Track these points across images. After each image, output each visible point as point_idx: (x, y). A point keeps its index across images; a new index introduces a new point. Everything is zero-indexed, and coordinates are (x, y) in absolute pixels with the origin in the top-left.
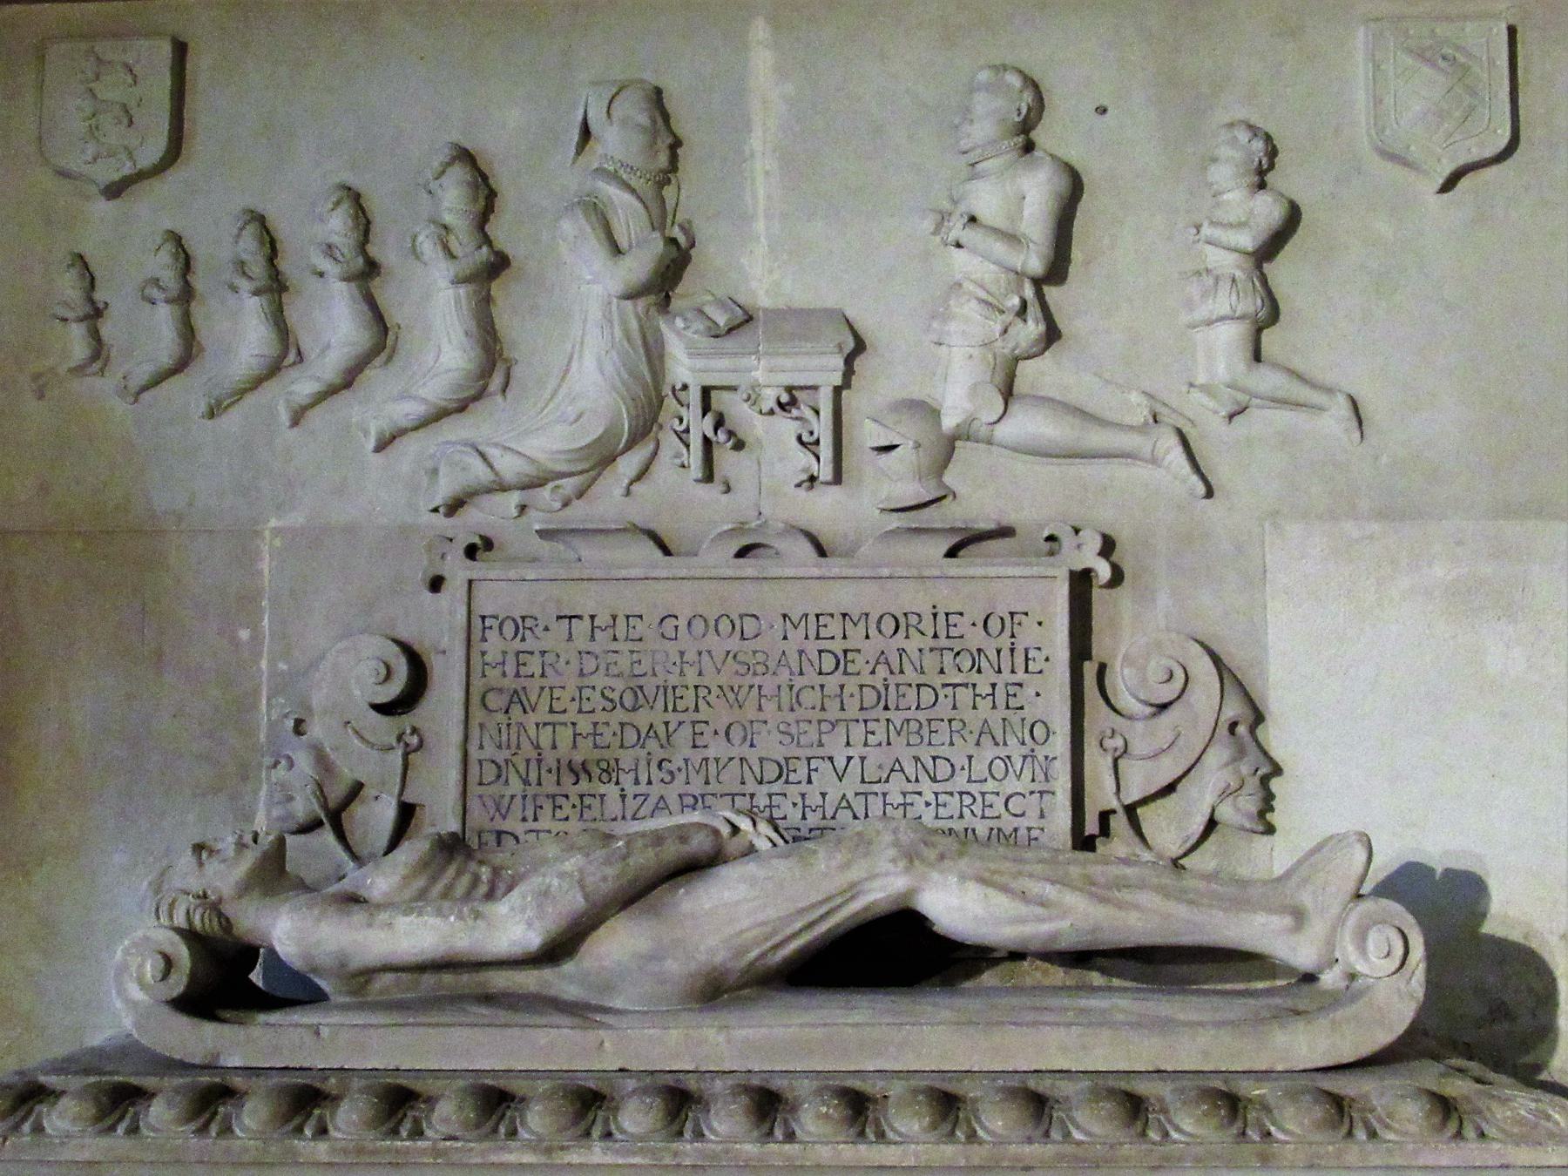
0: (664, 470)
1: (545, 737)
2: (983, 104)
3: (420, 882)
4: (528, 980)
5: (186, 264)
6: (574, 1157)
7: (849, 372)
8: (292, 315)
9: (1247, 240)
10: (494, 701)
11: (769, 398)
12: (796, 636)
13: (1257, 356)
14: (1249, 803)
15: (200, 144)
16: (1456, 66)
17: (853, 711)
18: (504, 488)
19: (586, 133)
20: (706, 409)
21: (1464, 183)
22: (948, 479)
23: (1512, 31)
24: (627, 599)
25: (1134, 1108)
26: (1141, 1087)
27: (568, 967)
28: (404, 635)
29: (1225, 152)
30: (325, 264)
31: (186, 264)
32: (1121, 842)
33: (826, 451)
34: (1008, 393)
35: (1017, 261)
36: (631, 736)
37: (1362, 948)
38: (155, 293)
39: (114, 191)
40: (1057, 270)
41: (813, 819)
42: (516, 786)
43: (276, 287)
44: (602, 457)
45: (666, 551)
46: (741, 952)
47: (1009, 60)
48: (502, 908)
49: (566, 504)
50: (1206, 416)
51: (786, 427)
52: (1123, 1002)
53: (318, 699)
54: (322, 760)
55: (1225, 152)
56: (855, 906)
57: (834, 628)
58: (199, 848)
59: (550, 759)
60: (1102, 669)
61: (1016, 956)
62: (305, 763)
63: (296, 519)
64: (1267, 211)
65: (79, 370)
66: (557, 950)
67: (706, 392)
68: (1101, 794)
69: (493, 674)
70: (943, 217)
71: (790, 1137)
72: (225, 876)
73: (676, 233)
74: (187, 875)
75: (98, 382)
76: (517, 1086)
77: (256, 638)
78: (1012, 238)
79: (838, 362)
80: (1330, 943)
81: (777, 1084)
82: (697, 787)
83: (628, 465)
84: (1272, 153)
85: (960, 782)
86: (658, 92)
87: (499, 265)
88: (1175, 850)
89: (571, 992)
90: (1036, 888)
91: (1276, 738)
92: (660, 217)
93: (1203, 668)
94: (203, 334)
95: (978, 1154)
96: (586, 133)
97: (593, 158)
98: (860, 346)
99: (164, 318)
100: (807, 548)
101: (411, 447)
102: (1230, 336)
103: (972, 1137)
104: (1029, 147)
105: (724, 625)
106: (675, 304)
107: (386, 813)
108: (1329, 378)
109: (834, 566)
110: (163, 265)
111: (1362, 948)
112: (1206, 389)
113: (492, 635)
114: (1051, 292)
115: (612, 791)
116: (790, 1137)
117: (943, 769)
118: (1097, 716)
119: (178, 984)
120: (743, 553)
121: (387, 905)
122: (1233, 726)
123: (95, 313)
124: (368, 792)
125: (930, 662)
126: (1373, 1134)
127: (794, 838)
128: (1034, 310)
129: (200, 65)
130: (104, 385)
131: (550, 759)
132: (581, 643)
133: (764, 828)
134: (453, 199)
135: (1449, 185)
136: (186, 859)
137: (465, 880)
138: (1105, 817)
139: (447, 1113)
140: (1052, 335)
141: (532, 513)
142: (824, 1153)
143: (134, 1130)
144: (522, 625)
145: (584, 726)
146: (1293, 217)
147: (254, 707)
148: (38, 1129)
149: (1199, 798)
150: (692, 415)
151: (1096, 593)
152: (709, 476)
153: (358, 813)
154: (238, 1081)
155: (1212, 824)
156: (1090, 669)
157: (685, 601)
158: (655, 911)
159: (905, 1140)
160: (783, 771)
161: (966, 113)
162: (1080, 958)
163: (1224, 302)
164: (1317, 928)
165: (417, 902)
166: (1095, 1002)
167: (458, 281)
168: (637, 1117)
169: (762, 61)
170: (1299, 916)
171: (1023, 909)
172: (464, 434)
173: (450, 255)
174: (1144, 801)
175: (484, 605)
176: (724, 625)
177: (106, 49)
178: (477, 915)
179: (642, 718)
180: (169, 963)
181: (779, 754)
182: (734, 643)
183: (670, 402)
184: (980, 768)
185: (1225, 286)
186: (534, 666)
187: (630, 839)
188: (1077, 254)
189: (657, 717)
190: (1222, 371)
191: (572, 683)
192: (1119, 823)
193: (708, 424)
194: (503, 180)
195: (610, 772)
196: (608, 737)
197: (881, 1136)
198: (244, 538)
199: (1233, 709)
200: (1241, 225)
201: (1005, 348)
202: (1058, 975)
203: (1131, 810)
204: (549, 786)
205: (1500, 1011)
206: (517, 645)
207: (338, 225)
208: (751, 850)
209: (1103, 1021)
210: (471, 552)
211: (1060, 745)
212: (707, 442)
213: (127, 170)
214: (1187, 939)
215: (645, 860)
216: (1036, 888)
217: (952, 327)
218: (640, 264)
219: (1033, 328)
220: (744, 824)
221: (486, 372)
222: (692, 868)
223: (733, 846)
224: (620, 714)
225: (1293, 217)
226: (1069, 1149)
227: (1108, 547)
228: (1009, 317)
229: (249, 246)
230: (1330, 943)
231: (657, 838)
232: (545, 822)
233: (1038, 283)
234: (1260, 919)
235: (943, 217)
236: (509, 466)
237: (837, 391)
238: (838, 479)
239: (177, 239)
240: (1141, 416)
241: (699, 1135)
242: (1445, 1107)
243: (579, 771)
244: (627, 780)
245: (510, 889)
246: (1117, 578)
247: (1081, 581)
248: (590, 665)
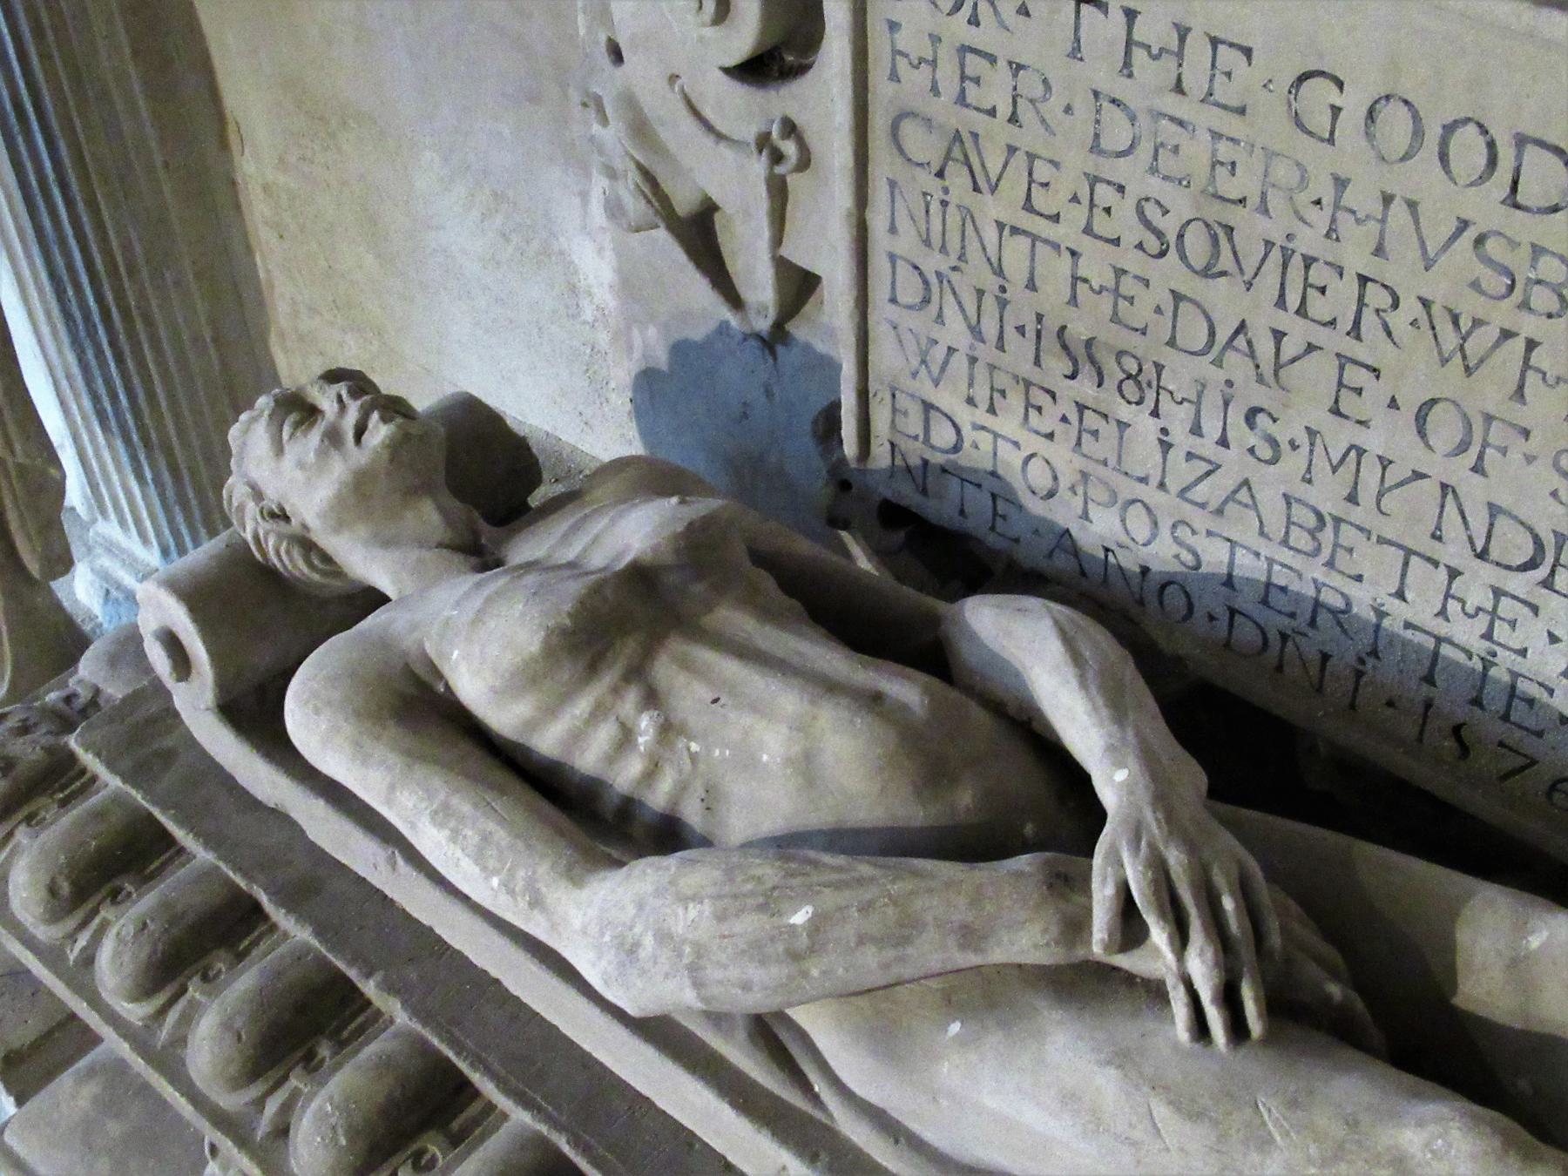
59: (1023, 308)
131: (1023, 308)
145: (1096, 268)
176: (1468, 150)
179: (1226, 301)
182: (1485, 206)
224: (1169, 273)
244: (1178, 418)
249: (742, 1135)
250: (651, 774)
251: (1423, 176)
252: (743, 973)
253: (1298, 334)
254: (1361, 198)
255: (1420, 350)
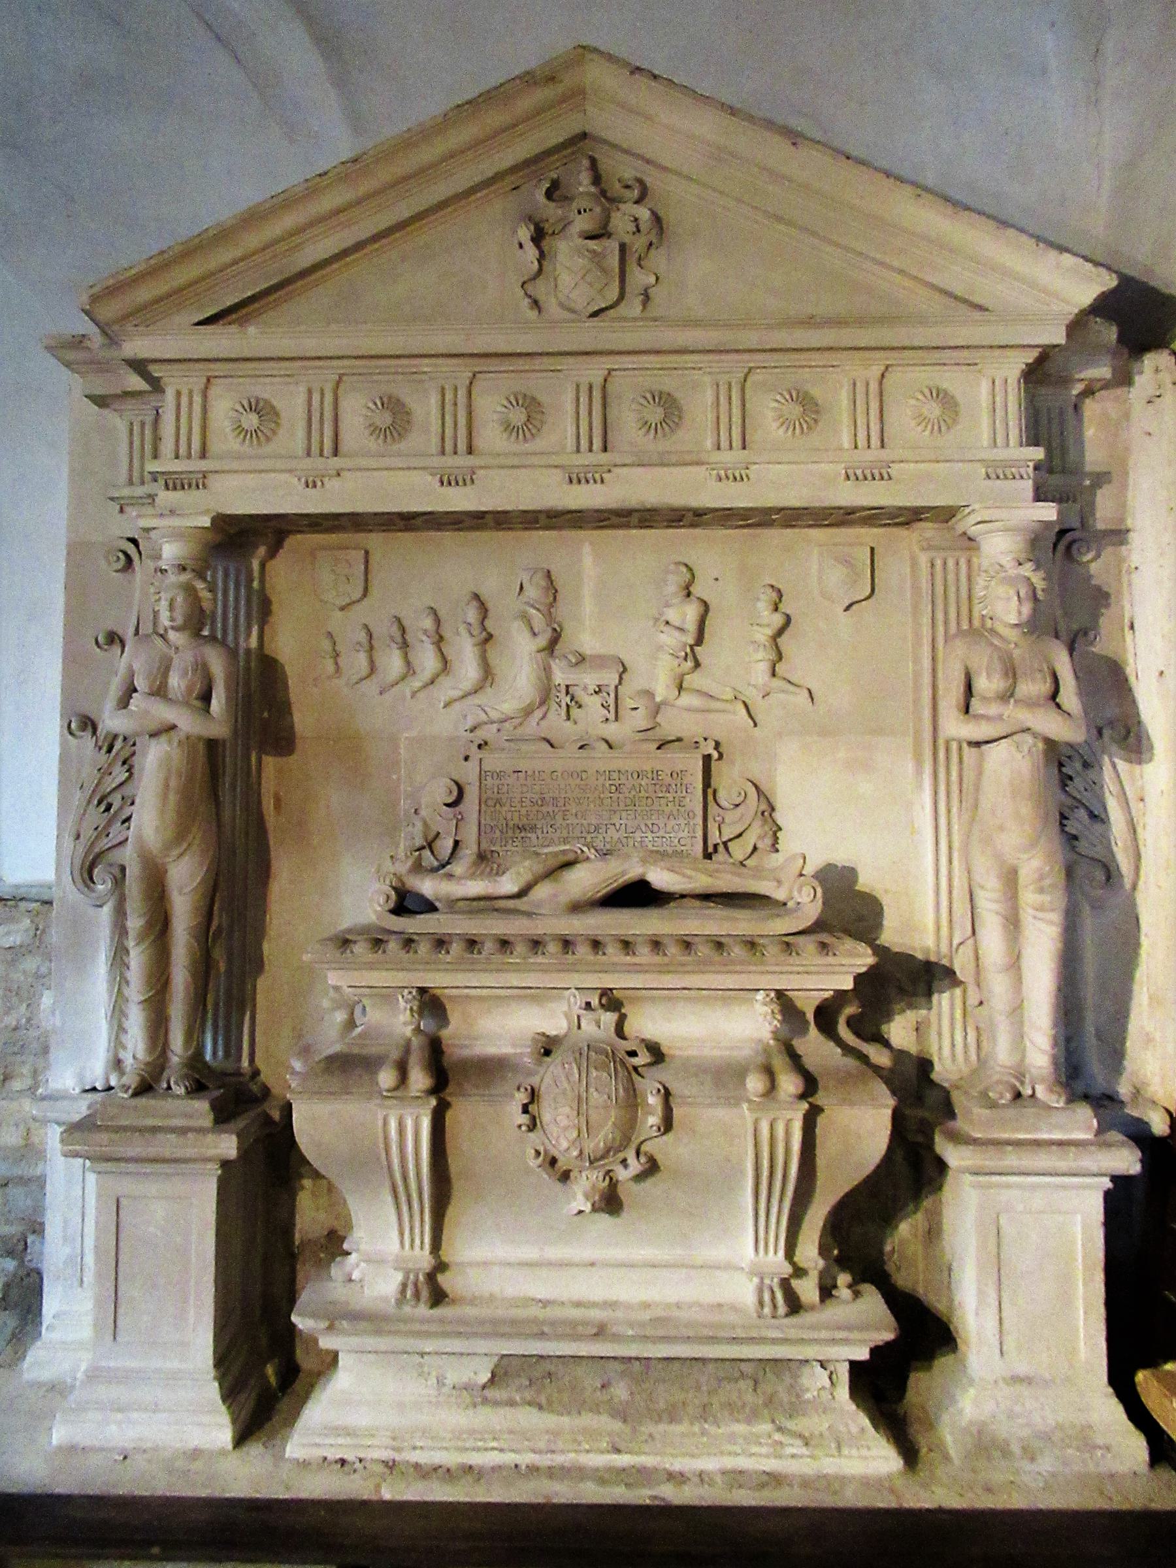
0: (550, 715)
1: (509, 816)
2: (672, 578)
3: (471, 871)
4: (511, 904)
5: (370, 636)
6: (532, 960)
7: (621, 678)
8: (411, 657)
9: (769, 632)
10: (490, 803)
11: (591, 688)
12: (601, 779)
13: (774, 674)
14: (768, 841)
15: (374, 591)
16: (847, 562)
17: (622, 806)
18: (492, 722)
19: (521, 588)
20: (567, 693)
21: (854, 607)
22: (658, 719)
23: (872, 549)
24: (538, 765)
25: (719, 946)
26: (723, 940)
27: (525, 899)
28: (456, 778)
29: (762, 596)
30: (424, 638)
31: (370, 636)
32: (721, 856)
33: (612, 709)
34: (680, 688)
35: (684, 639)
36: (540, 816)
37: (800, 891)
38: (358, 647)
39: (342, 609)
40: (699, 640)
41: (608, 847)
42: (498, 833)
43: (405, 645)
44: (528, 712)
45: (552, 746)
46: (585, 895)
47: (681, 559)
48: (504, 878)
49: (515, 728)
50: (752, 695)
51: (597, 700)
52: (719, 912)
53: (424, 801)
54: (426, 824)
55: (762, 596)
56: (626, 877)
57: (615, 776)
58: (392, 857)
59: (511, 824)
60: (715, 792)
61: (683, 896)
62: (419, 826)
63: (413, 734)
64: (778, 620)
65: (329, 678)
66: (522, 894)
67: (567, 686)
68: (714, 837)
69: (489, 792)
70: (657, 620)
71: (604, 954)
72: (403, 868)
73: (556, 626)
74: (388, 866)
75: (337, 681)
76: (512, 939)
77: (399, 779)
78: (681, 630)
79: (617, 676)
80: (791, 891)
81: (600, 938)
82: (565, 834)
83: (538, 714)
84: (780, 594)
85: (661, 833)
86: (549, 572)
87: (490, 637)
88: (741, 858)
89: (524, 908)
90: (689, 872)
91: (779, 817)
92: (549, 616)
93: (752, 791)
94: (377, 664)
95: (666, 960)
96: (521, 588)
97: (523, 598)
98: (625, 670)
99: (362, 659)
100: (605, 746)
101: (457, 706)
102: (763, 668)
103: (665, 955)
104: (689, 595)
105: (575, 775)
106: (556, 653)
107: (450, 843)
108: (801, 682)
109: (614, 754)
110: (362, 636)
111: (800, 891)
112: (755, 686)
113: (489, 778)
114: (697, 649)
115: (533, 836)
116: (604, 954)
117: (655, 828)
118: (713, 809)
119: (391, 904)
120: (581, 747)
121: (460, 878)
122: (763, 813)
123: (336, 655)
124: (442, 835)
125: (651, 788)
126: (798, 954)
127: (605, 854)
128: (690, 656)
129: (375, 559)
130: (340, 682)
131: (511, 824)
132: (522, 781)
133: (593, 851)
134: (472, 615)
135: (847, 609)
136: (389, 862)
137: (488, 870)
138: (716, 846)
139: (489, 946)
140: (697, 665)
141: (502, 732)
142: (615, 959)
143: (384, 952)
144: (499, 775)
145: (523, 811)
146: (788, 620)
147: (399, 804)
148: (352, 952)
149: (750, 839)
150: (562, 695)
151: (713, 764)
152: (568, 718)
153: (437, 844)
154: (415, 937)
155: (755, 848)
156: (710, 791)
157: (558, 765)
158: (556, 880)
159: (642, 955)
160: (597, 829)
161: (665, 581)
162: (706, 897)
163: (761, 655)
164: (786, 885)
165: (472, 876)
166: (707, 912)
167: (475, 645)
168: (553, 948)
169: (588, 561)
170: (779, 882)
171: (686, 880)
172: (477, 701)
173: (472, 635)
174: (730, 840)
175: (485, 767)
176: (575, 775)
177: (341, 554)
178: (496, 881)
179: (544, 809)
180: (388, 897)
181: (594, 822)
182: (578, 781)
183: (554, 691)
184: (669, 829)
185: (761, 648)
186: (505, 789)
187: (546, 854)
188: (706, 636)
189: (550, 809)
190: (761, 681)
191: (518, 796)
192: (721, 848)
193: (568, 699)
194: (490, 605)
195: (533, 828)
196: (532, 816)
197: (634, 954)
198: (393, 740)
199: (764, 806)
200: (768, 625)
201: (679, 670)
202: (697, 903)
203: (725, 844)
204: (510, 834)
205: (861, 919)
206: (498, 782)
207: (428, 623)
208: (588, 858)
209: (709, 917)
210: (480, 746)
211: (699, 820)
212: (568, 705)
213: (348, 600)
214: (741, 890)
215: (552, 863)
216: (689, 872)
217: (659, 663)
218: (542, 641)
219: (690, 664)
220: (585, 849)
221: (485, 679)
222: (568, 864)
223: (581, 857)
224: (536, 808)
225: (788, 620)
226: (696, 958)
227: (717, 745)
228: (681, 660)
229: (395, 631)
230: (791, 891)
231: (555, 854)
232: (509, 847)
233: (691, 647)
234: (765, 883)
235: (657, 620)
236: (494, 715)
237: (616, 687)
238: (617, 719)
239: (366, 626)
240: (730, 696)
241: (573, 953)
242: (823, 946)
243: (522, 829)
244: (539, 832)
245: (504, 873)
246: (721, 756)
247: (707, 759)
248: (525, 789)
249: (114, 1427)
250: (952, 999)
251: (570, 781)
252: (611, 1001)
253: (556, 810)
254: (562, 786)
255: (574, 805)
